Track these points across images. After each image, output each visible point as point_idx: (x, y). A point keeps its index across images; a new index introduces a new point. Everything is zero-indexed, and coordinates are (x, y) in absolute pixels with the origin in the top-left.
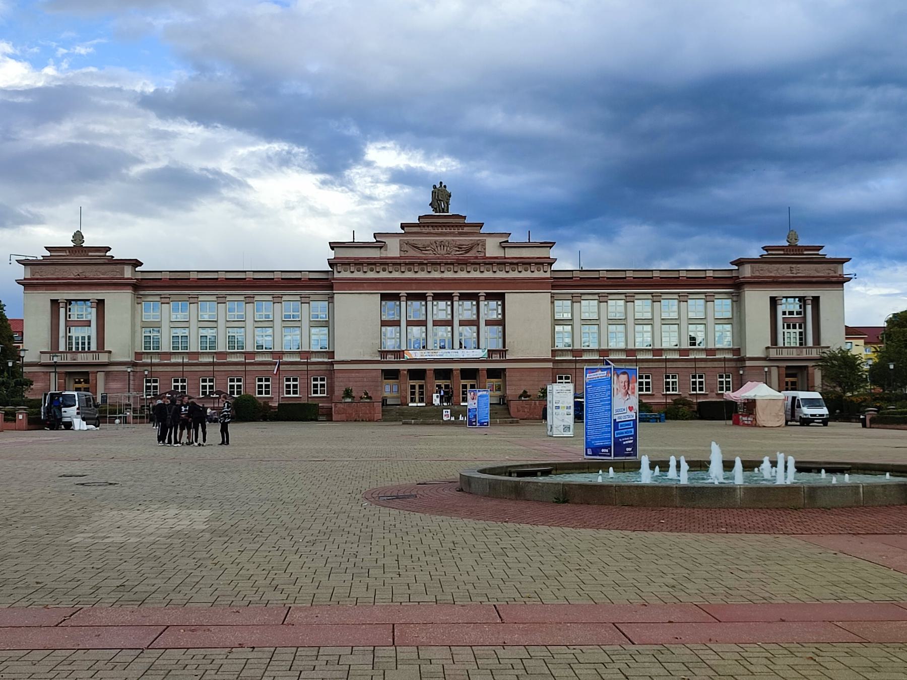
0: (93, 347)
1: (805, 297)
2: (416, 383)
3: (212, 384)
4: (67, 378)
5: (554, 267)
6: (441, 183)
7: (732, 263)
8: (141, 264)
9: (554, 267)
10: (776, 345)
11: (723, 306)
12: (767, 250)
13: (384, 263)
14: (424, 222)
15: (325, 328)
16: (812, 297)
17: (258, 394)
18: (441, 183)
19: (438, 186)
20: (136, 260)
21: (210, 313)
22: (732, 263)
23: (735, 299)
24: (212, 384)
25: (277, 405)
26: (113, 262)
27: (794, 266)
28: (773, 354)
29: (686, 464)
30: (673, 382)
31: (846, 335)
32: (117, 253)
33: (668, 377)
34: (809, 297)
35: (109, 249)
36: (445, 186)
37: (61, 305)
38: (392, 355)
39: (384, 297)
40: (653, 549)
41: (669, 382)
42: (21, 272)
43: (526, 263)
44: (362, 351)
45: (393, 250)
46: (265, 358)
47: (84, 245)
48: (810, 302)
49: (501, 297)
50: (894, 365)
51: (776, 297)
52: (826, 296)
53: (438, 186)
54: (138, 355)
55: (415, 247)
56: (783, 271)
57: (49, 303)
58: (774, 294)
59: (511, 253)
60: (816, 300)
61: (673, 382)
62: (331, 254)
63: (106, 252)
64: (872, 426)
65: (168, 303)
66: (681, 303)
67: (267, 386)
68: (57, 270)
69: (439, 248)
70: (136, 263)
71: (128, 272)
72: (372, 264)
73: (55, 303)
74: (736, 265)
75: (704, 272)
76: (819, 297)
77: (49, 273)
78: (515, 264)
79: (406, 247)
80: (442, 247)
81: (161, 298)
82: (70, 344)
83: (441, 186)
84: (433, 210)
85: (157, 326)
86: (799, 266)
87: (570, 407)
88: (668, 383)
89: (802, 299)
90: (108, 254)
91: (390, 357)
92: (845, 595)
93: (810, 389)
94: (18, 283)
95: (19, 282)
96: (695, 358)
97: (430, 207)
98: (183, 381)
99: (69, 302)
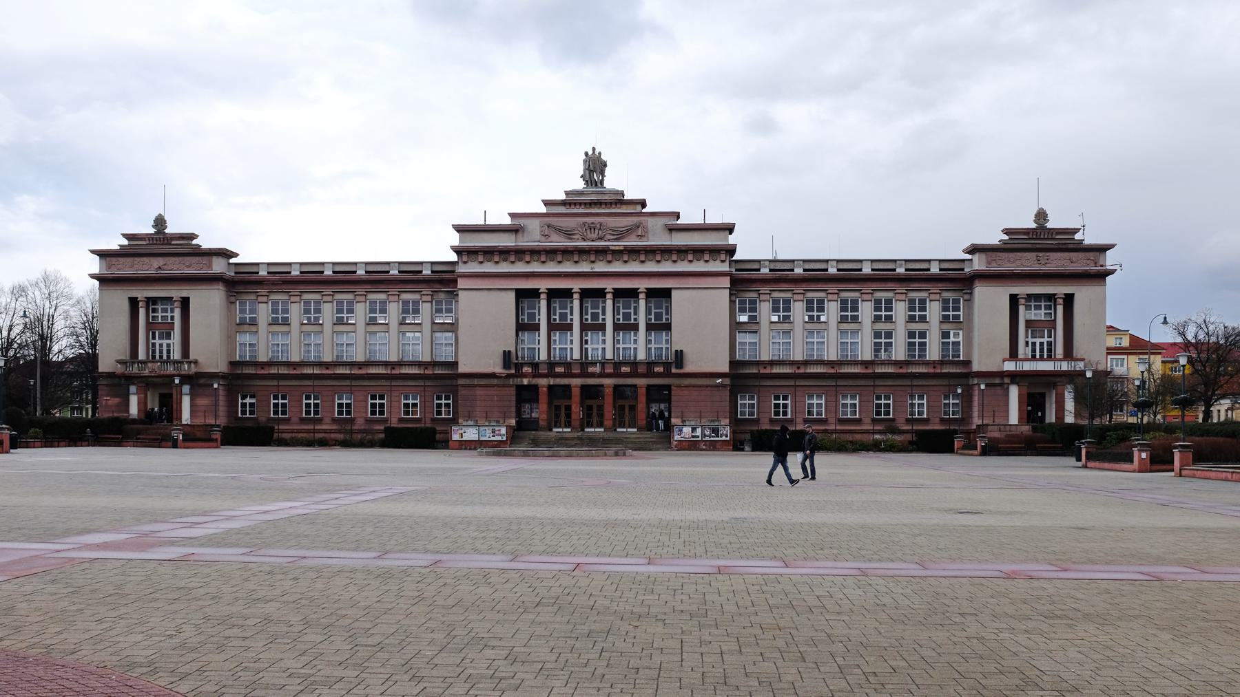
3: (349, 402)
4: (149, 394)
6: (594, 149)
8: (236, 255)
13: (519, 253)
14: (572, 201)
15: (450, 334)
16: (1065, 294)
17: (437, 415)
18: (594, 149)
19: (590, 153)
21: (751, 314)
25: (779, 428)
26: (1080, 248)
27: (1041, 254)
33: (373, 398)
34: (1061, 294)
36: (600, 153)
37: (141, 304)
38: (529, 367)
42: (95, 265)
44: (492, 361)
45: (533, 237)
46: (412, 370)
47: (1049, 225)
48: (1061, 301)
49: (666, 293)
51: (1018, 295)
52: (1083, 295)
53: (590, 153)
54: (233, 364)
55: (559, 230)
56: (1028, 263)
57: (127, 299)
58: (134, 295)
59: (680, 240)
64: (1089, 464)
66: (898, 302)
68: (135, 262)
69: (588, 231)
71: (218, 266)
72: (504, 253)
75: (322, 266)
76: (1073, 295)
77: (126, 268)
80: (593, 230)
81: (794, 294)
83: (594, 152)
85: (437, 328)
86: (1048, 254)
87: (217, 439)
90: (194, 242)
91: (625, 369)
92: (1191, 683)
95: (93, 276)
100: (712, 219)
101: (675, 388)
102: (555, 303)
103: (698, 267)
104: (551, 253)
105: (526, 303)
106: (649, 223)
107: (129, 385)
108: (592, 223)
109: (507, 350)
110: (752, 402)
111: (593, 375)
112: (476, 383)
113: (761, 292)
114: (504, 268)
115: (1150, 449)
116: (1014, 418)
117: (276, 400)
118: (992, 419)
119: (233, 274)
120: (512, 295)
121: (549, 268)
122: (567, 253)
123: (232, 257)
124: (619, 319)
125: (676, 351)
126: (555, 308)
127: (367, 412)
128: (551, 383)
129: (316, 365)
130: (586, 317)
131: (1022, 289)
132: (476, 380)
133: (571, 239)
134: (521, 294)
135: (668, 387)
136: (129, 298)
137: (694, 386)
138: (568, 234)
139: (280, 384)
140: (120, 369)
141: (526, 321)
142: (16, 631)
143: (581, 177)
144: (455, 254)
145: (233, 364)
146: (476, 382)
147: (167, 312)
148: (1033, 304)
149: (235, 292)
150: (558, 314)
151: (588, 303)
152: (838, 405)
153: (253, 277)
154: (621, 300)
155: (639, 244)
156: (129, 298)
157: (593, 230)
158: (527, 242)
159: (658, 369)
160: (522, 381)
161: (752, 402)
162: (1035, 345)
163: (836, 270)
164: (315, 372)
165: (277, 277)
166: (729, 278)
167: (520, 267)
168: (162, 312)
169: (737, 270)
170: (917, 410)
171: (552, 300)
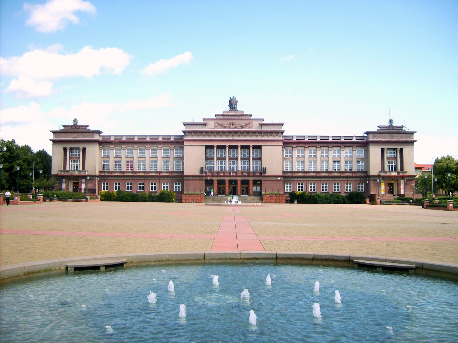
0: (81, 169)
2: (245, 186)
5: (284, 134)
6: (233, 96)
7: (364, 133)
9: (284, 134)
10: (403, 170)
11: (360, 153)
12: (379, 127)
13: (207, 133)
18: (233, 96)
19: (232, 98)
20: (99, 131)
22: (364, 133)
28: (382, 174)
29: (11, 140)
30: (118, 186)
31: (20, 201)
32: (92, 128)
33: (335, 184)
36: (235, 98)
39: (207, 147)
43: (271, 133)
45: (211, 127)
47: (78, 124)
48: (399, 151)
49: (260, 147)
53: (232, 98)
58: (383, 147)
59: (265, 129)
60: (401, 150)
61: (118, 186)
62: (184, 128)
65: (113, 150)
67: (155, 187)
70: (99, 132)
72: (201, 133)
74: (366, 134)
77: (63, 137)
78: (266, 133)
82: (71, 167)
88: (323, 187)
89: (395, 150)
95: (51, 140)
96: (347, 176)
98: (131, 184)
99: (71, 149)
103: (271, 138)
104: (218, 133)
119: (101, 139)
120: (204, 147)
123: (101, 133)
128: (218, 179)
138: (224, 126)
140: (60, 173)
145: (284, 172)
146: (190, 178)
153: (168, 141)
155: (250, 130)
165: (118, 140)
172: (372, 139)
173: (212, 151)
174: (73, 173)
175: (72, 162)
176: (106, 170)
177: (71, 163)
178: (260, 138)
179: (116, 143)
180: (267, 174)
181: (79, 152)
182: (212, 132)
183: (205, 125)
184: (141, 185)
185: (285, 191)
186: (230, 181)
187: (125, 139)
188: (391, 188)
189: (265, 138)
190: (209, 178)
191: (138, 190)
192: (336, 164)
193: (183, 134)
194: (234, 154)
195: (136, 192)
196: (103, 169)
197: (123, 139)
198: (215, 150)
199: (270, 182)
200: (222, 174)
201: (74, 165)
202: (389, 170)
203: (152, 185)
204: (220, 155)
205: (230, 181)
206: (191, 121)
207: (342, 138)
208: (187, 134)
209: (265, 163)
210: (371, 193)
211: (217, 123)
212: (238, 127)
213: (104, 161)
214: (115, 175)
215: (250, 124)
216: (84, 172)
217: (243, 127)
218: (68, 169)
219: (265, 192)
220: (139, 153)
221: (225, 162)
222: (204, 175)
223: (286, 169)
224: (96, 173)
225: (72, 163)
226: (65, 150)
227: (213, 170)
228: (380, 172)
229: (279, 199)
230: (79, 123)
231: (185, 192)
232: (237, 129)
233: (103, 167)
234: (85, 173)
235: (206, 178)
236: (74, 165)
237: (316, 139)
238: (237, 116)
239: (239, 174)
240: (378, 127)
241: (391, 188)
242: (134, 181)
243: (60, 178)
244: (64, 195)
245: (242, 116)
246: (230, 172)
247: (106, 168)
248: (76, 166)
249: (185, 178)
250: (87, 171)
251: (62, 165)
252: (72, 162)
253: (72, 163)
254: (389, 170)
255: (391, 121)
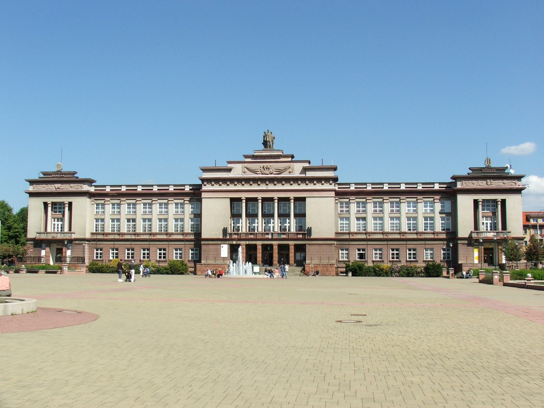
1: (496, 199)
3: (165, 252)
8: (94, 181)
10: (506, 230)
13: (232, 181)
23: (453, 200)
24: (165, 252)
35: (76, 173)
40: (525, 365)
41: (98, 253)
46: (162, 237)
49: (303, 199)
50: (452, 244)
54: (337, 233)
63: (74, 175)
72: (225, 181)
73: (476, 202)
78: (312, 180)
79: (246, 170)
80: (267, 169)
82: (54, 228)
84: (264, 147)
89: (495, 201)
90: (75, 176)
93: (223, 258)
94: (26, 192)
97: (263, 145)
100: (326, 164)
101: (308, 246)
102: (249, 204)
103: (319, 186)
104: (247, 181)
105: (235, 203)
106: (295, 166)
107: (42, 244)
108: (267, 166)
109: (225, 227)
110: (449, 252)
111: (268, 239)
112: (210, 243)
113: (367, 198)
114: (224, 187)
115: (509, 275)
116: (476, 261)
117: (148, 251)
118: (466, 261)
119: (94, 191)
120: (229, 200)
121: (239, 187)
122: (255, 181)
124: (265, 212)
125: (308, 227)
126: (265, 206)
127: (157, 257)
128: (247, 243)
129: (133, 234)
130: (280, 211)
131: (480, 197)
132: (210, 242)
133: (257, 173)
134: (232, 200)
135: (305, 245)
136: (44, 202)
137: (317, 244)
138: (255, 172)
139: (115, 243)
140: (38, 236)
141: (251, 213)
142: (146, 361)
143: (262, 144)
144: (201, 181)
145: (337, 233)
146: (210, 242)
147: (61, 209)
148: (486, 204)
149: (94, 199)
150: (266, 209)
151: (250, 204)
152: (388, 254)
153: (103, 192)
154: (282, 202)
155: (290, 176)
156: (44, 202)
157: (267, 169)
158: (236, 175)
159: (300, 236)
160: (233, 242)
161: (449, 252)
162: (487, 224)
163: (388, 188)
164: (132, 238)
165: (115, 192)
166: (334, 192)
167: (232, 187)
168: (59, 209)
169: (339, 188)
170: (446, 256)
171: (248, 202)
172: (460, 187)
173: (288, 205)
174: (55, 235)
175: (54, 221)
176: (100, 232)
177: (53, 223)
178: (303, 187)
179: (113, 195)
180: (313, 236)
181: (64, 208)
182: (239, 180)
183: (229, 170)
184: (395, 252)
185: (340, 259)
186: (264, 247)
187: (141, 190)
188: (491, 255)
189: (311, 186)
190: (234, 242)
191: (391, 259)
192: (361, 222)
193: (451, 181)
194: (286, 209)
195: (439, 261)
196: (96, 231)
197: (122, 190)
198: (276, 204)
199: (317, 247)
200: (252, 236)
201: (58, 225)
202: (487, 229)
203: (144, 252)
204: (282, 211)
205: (264, 247)
206: (211, 165)
207: (420, 186)
208: (205, 183)
209: (310, 222)
210: (460, 262)
211: (246, 168)
212: (274, 173)
213: (97, 220)
214: (110, 238)
215: (289, 168)
216: (70, 234)
217: (280, 172)
218: (49, 230)
219: (310, 261)
220: (341, 207)
221: (257, 220)
222: (228, 237)
223: (341, 230)
224: (85, 235)
225: (54, 223)
226: (46, 205)
227: (289, 230)
228: (471, 232)
229: (327, 270)
230: (493, 165)
231: (307, 261)
232: (272, 176)
233: (96, 228)
234: (71, 235)
235: (231, 242)
236: (58, 225)
237: (383, 188)
238: (258, 158)
239: (243, 237)
240: (470, 169)
241: (491, 255)
242: (152, 245)
243: (38, 243)
244: (90, 265)
245: (279, 157)
246: (246, 234)
247: (100, 229)
248: (60, 226)
249: (202, 242)
250: (74, 233)
251: (41, 226)
252: (54, 221)
253: (54, 223)
254: (487, 229)
255: (489, 161)
